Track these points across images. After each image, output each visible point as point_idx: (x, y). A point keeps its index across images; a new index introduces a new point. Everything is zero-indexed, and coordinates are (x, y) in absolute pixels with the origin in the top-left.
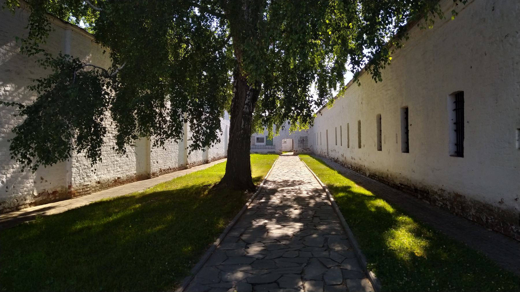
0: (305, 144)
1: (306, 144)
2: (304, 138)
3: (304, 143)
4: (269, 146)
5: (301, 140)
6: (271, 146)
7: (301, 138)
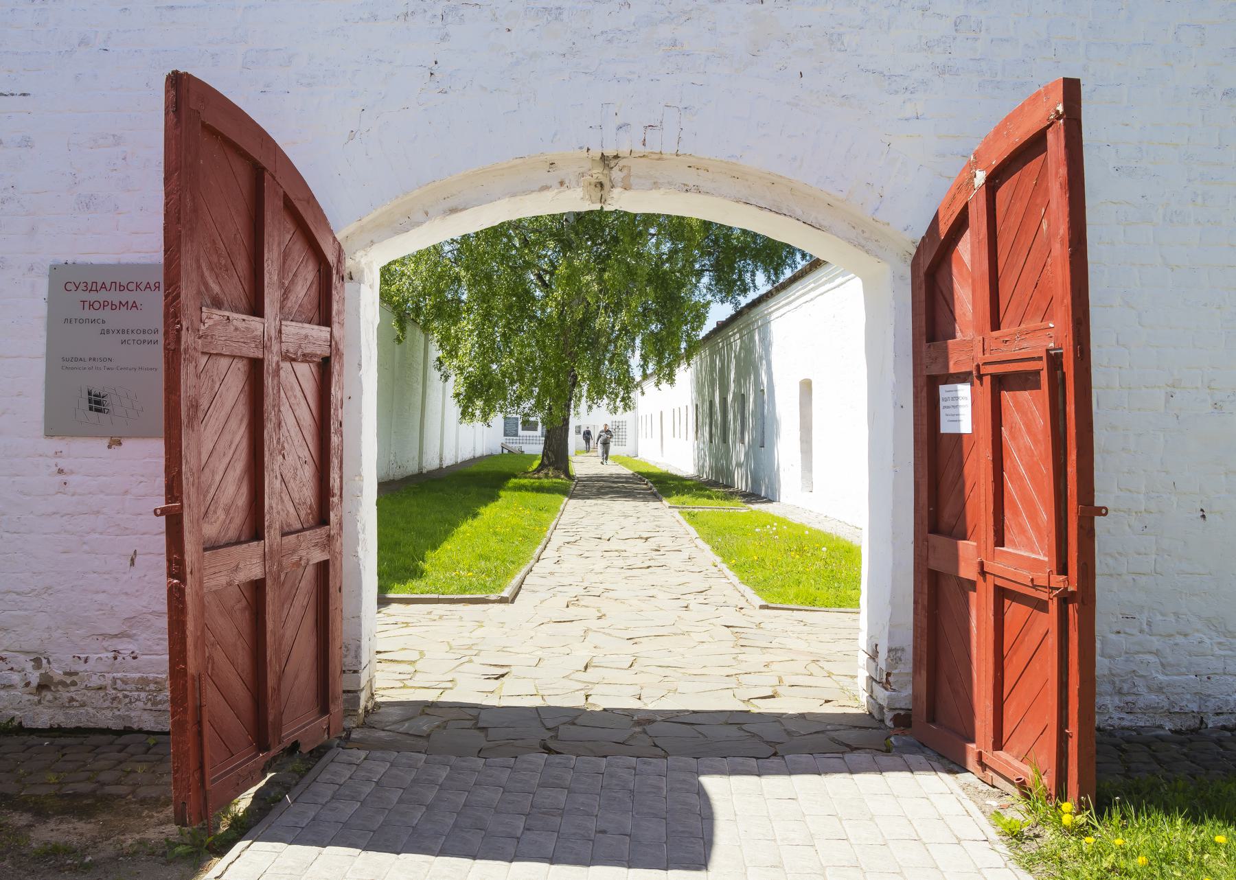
2: (621, 424)
3: (620, 434)
4: (511, 438)
6: (515, 438)
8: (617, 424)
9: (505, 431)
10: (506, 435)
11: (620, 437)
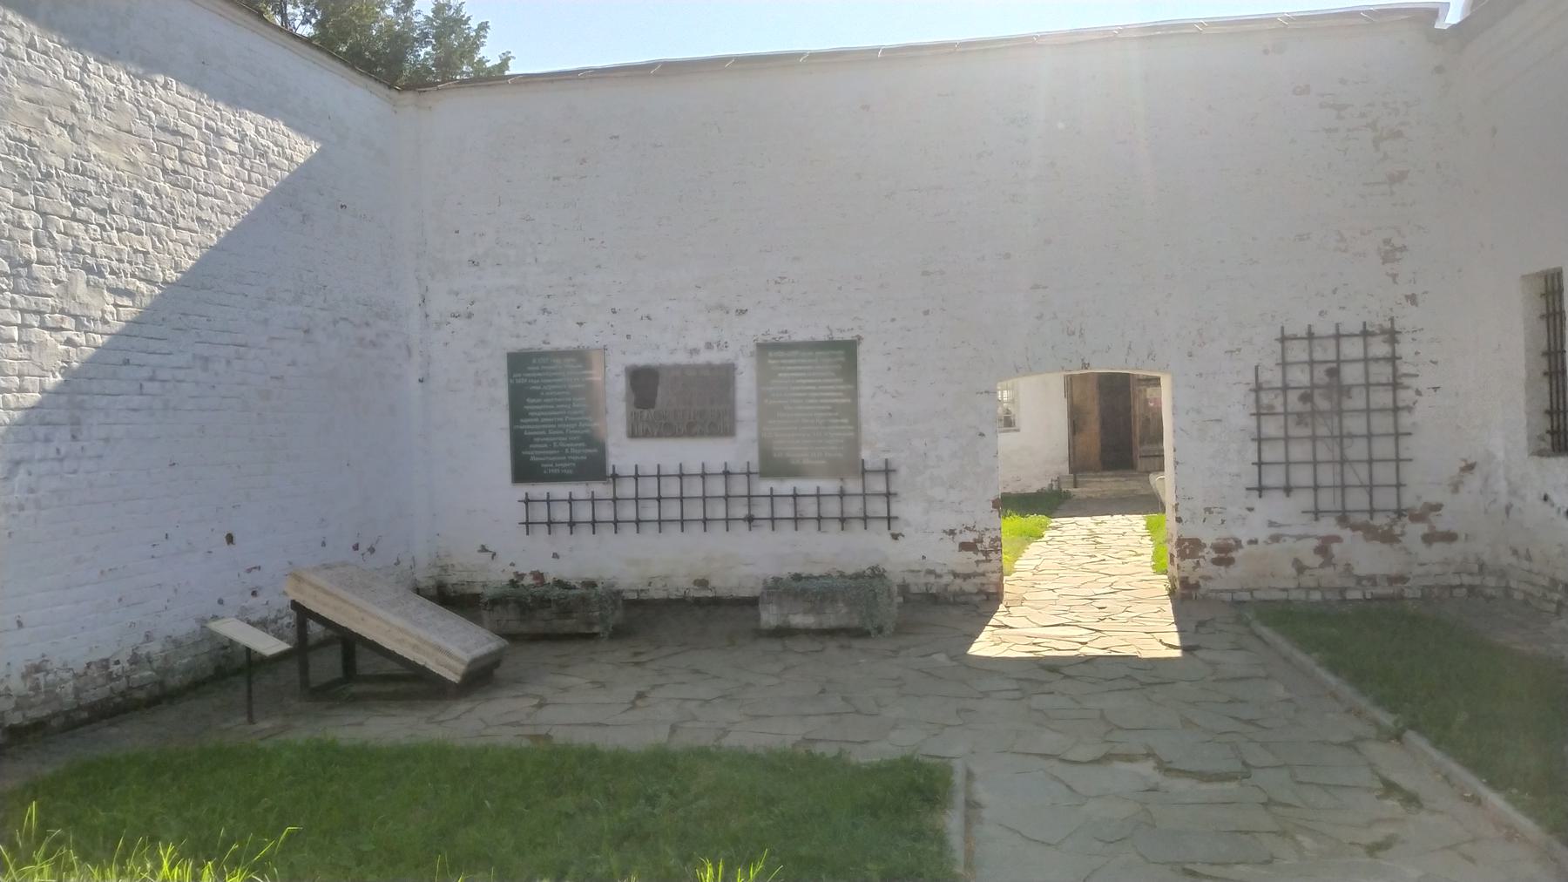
0: (1357, 450)
1: (1383, 448)
2: (1353, 349)
3: (1355, 424)
4: (560, 490)
5: (1300, 377)
6: (580, 490)
7: (1298, 352)
8: (1325, 352)
9: (519, 442)
10: (524, 471)
11: (1357, 450)
